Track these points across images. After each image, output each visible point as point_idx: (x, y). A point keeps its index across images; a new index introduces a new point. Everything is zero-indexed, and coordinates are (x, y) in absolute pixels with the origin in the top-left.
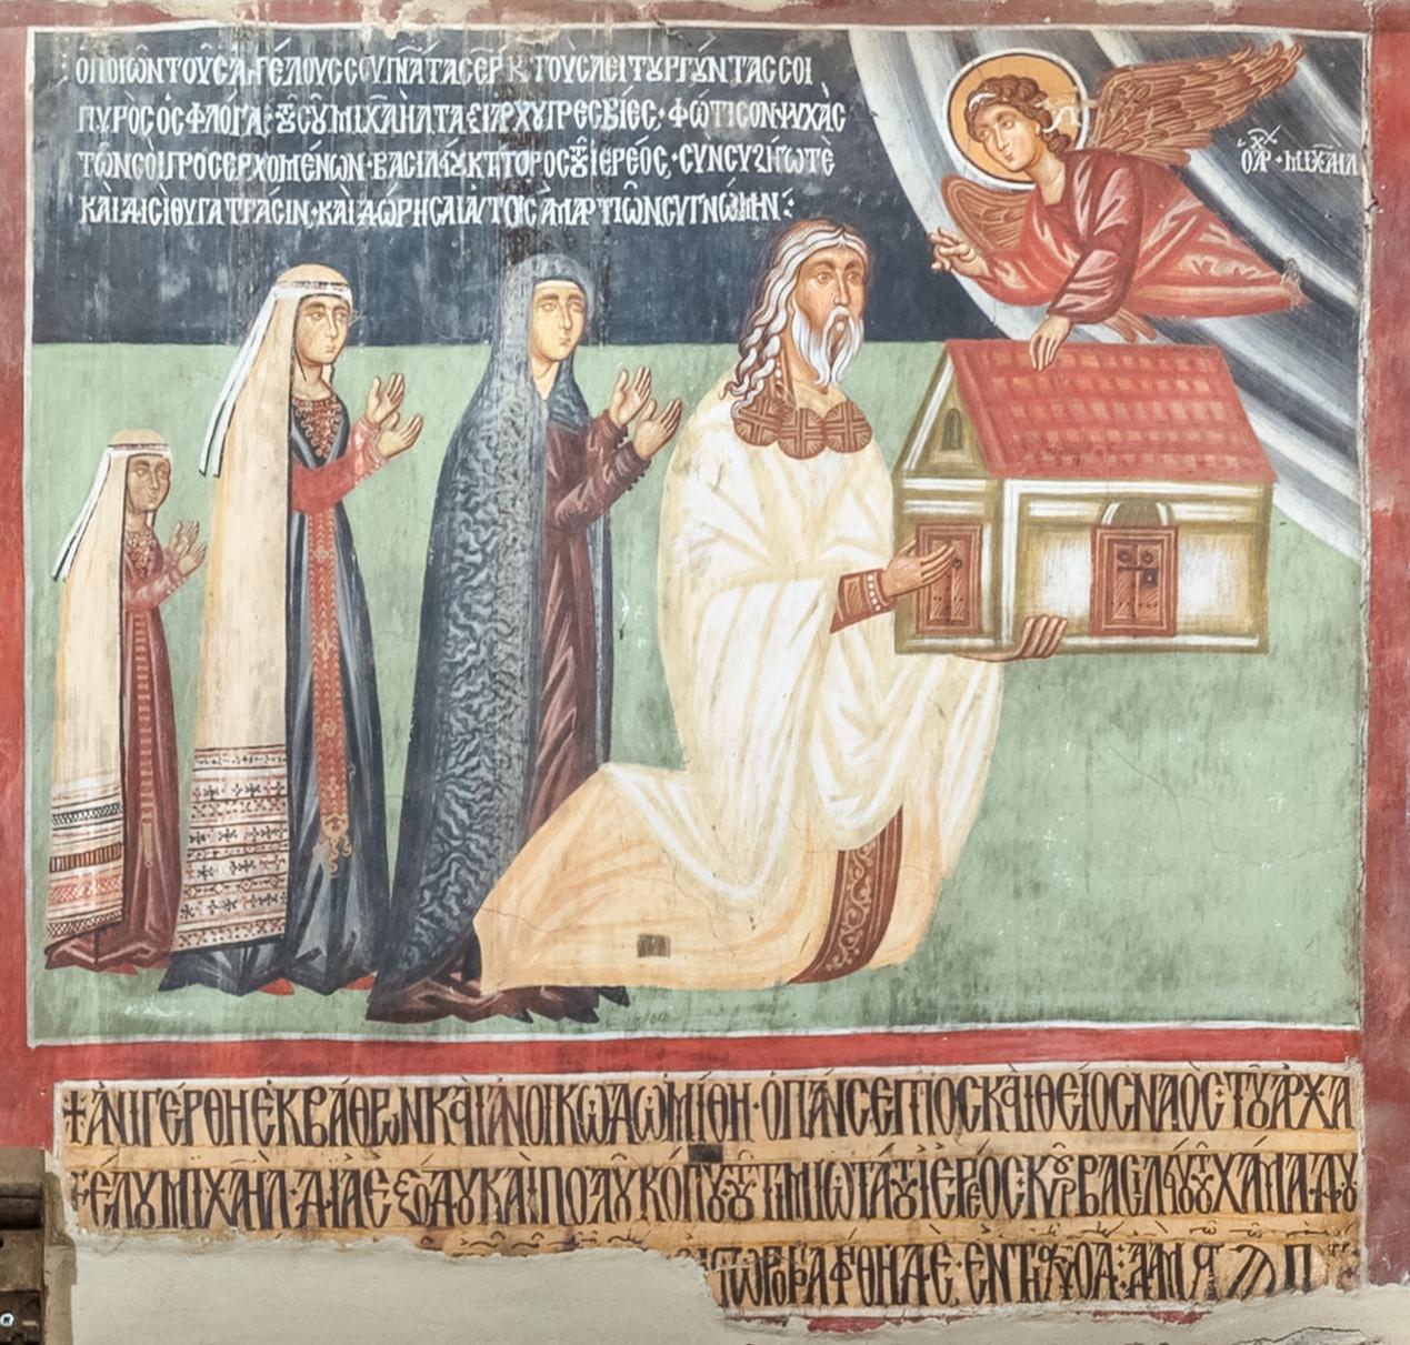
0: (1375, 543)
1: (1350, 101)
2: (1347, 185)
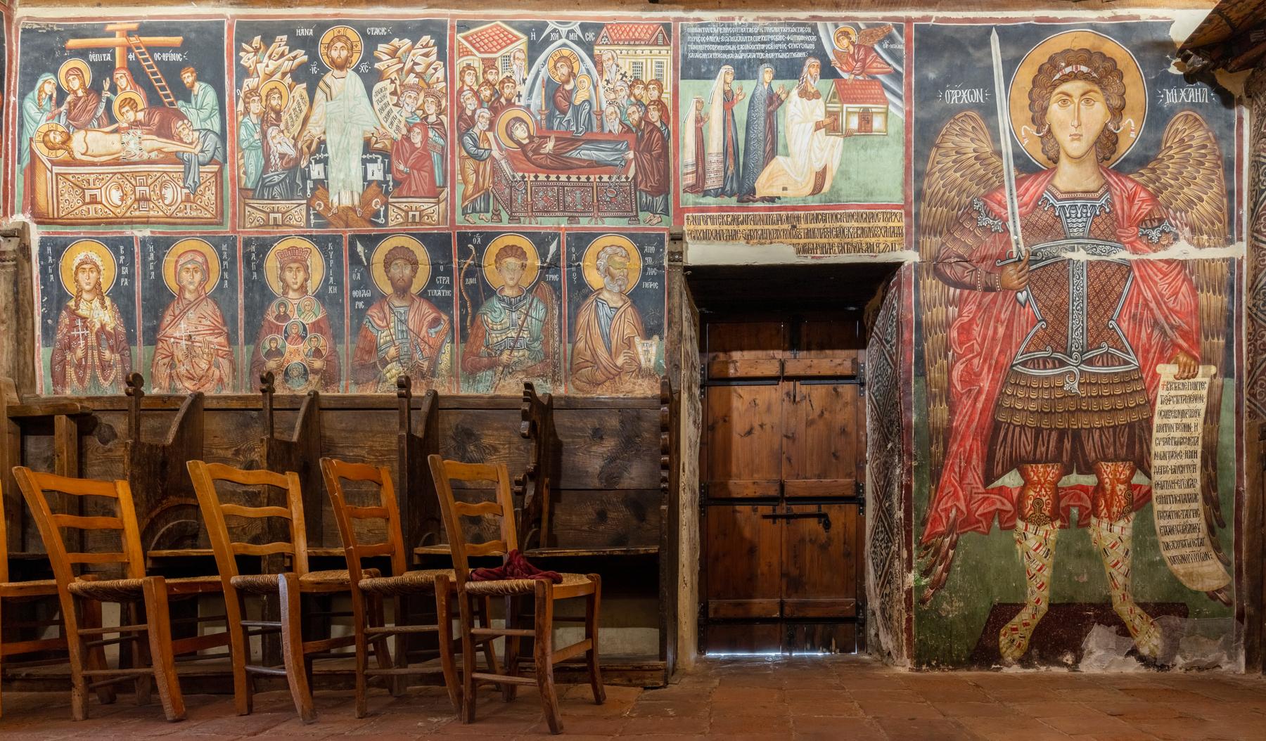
2: (901, 50)
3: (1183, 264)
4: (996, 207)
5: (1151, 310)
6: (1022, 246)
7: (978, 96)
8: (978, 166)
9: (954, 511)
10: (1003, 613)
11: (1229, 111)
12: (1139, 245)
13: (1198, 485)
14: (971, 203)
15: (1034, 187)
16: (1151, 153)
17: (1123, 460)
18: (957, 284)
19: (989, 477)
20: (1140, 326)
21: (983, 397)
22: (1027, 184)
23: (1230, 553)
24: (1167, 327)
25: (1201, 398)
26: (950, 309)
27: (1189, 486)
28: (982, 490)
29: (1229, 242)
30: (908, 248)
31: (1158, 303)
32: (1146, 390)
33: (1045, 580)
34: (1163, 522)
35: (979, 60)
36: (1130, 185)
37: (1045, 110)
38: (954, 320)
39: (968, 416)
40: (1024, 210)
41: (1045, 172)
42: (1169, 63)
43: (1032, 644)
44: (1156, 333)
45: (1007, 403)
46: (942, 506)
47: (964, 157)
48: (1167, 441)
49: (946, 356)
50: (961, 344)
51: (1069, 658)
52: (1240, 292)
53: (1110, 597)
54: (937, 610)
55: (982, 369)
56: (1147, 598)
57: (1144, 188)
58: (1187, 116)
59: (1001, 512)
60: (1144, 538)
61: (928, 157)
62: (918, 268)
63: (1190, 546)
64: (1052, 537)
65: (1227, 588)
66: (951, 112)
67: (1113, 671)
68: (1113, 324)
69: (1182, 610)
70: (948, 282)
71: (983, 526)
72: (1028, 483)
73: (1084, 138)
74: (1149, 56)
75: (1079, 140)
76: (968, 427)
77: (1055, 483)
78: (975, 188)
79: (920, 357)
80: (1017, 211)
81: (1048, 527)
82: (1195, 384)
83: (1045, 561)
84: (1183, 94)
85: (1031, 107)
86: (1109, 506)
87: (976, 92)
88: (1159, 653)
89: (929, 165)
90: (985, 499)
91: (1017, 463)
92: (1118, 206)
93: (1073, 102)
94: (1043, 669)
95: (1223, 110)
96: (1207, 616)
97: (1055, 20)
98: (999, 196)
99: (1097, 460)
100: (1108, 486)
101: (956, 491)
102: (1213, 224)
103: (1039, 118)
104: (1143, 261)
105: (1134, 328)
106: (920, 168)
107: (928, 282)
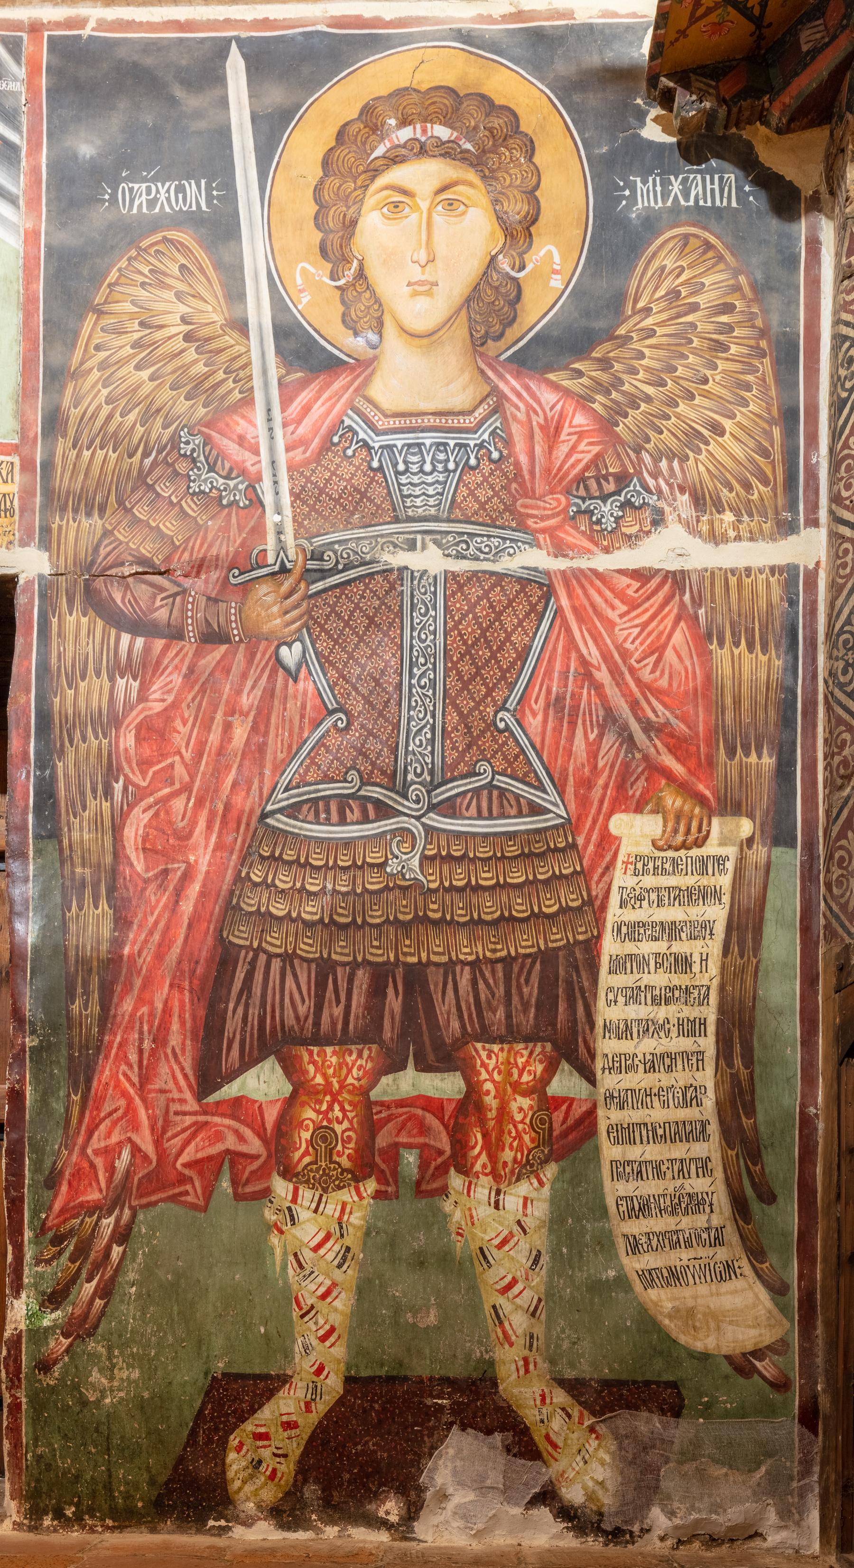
0: (26, 241)
1: (18, 61)
2: (14, 94)
3: (677, 580)
4: (231, 448)
5: (599, 687)
6: (289, 538)
7: (195, 195)
8: (191, 354)
9: (126, 1154)
10: (234, 1397)
11: (787, 227)
12: (571, 536)
13: (709, 1102)
14: (175, 441)
15: (323, 404)
16: (600, 324)
17: (527, 1039)
18: (136, 627)
19: (208, 1077)
20: (573, 724)
21: (195, 889)
22: (304, 397)
23: (786, 1265)
24: (635, 726)
25: (716, 894)
26: (121, 682)
27: (686, 1103)
28: (192, 1105)
29: (788, 528)
30: (23, 544)
31: (614, 671)
32: (584, 874)
33: (336, 1319)
34: (624, 1188)
35: (198, 115)
36: (548, 397)
37: (350, 226)
38: (129, 707)
39: (164, 928)
40: (298, 455)
41: (353, 369)
42: (641, 116)
43: (303, 1471)
44: (609, 740)
45: (250, 904)
46: (97, 1142)
47: (159, 335)
48: (633, 995)
49: (108, 792)
50: (144, 764)
51: (391, 1508)
52: (812, 645)
53: (491, 1363)
54: (76, 1387)
55: (193, 823)
56: (584, 1369)
57: (583, 401)
58: (686, 237)
59: (235, 1157)
60: (578, 1226)
61: (76, 334)
62: (47, 589)
63: (689, 1244)
64: (356, 1219)
65: (779, 1347)
66: (130, 234)
67: (501, 1540)
68: (506, 718)
69: (668, 1399)
70: (116, 620)
71: (194, 1191)
72: (301, 1090)
73: (442, 291)
74: (593, 100)
75: (429, 293)
76: (159, 956)
77: (365, 1092)
78: (182, 406)
79: (46, 795)
80: (282, 458)
81: (346, 1195)
82: (703, 862)
83: (338, 1275)
84: (676, 187)
85: (318, 220)
86: (492, 1148)
87: (191, 188)
88: (607, 1501)
89: (78, 354)
90: (200, 1127)
91: (276, 1042)
92: (520, 447)
93: (415, 208)
94: (331, 1531)
95: (774, 223)
96: (727, 1414)
97: (377, 22)
98: (241, 426)
99: (466, 1038)
100: (490, 1101)
101: (130, 1108)
102: (747, 487)
103: (337, 245)
104: (579, 575)
105: (557, 730)
106: (56, 359)
107: (71, 620)
